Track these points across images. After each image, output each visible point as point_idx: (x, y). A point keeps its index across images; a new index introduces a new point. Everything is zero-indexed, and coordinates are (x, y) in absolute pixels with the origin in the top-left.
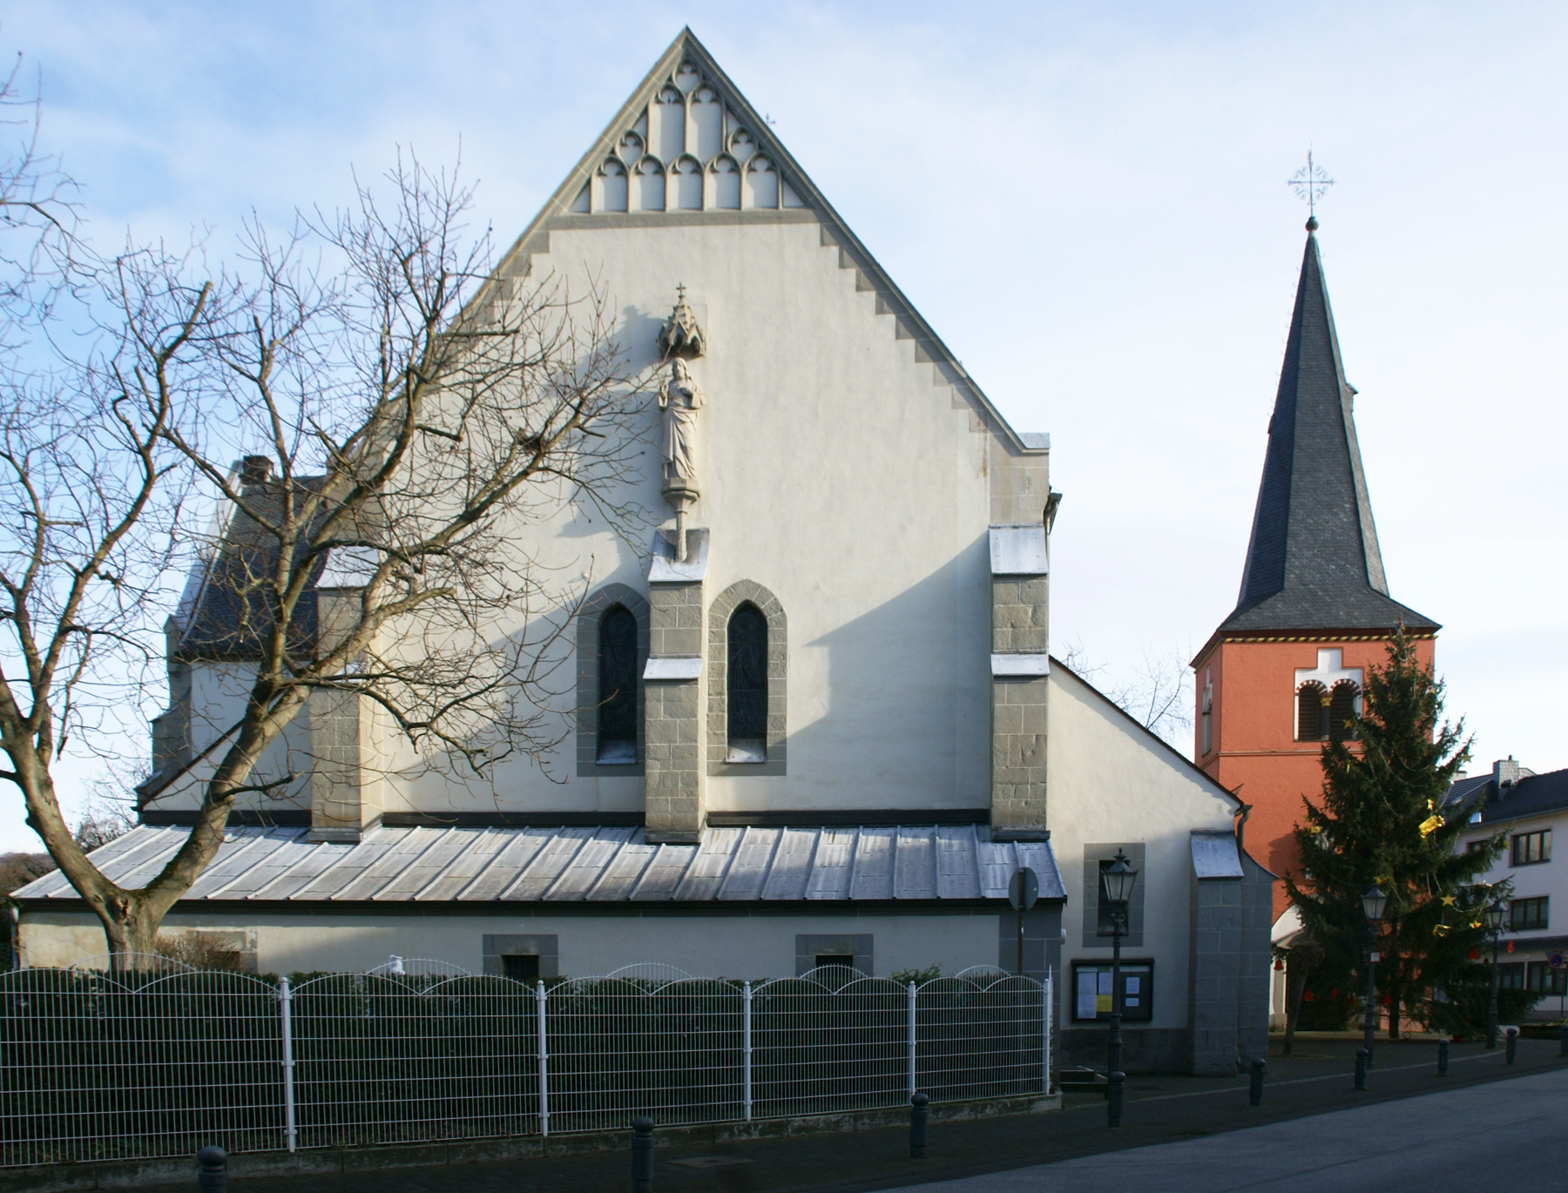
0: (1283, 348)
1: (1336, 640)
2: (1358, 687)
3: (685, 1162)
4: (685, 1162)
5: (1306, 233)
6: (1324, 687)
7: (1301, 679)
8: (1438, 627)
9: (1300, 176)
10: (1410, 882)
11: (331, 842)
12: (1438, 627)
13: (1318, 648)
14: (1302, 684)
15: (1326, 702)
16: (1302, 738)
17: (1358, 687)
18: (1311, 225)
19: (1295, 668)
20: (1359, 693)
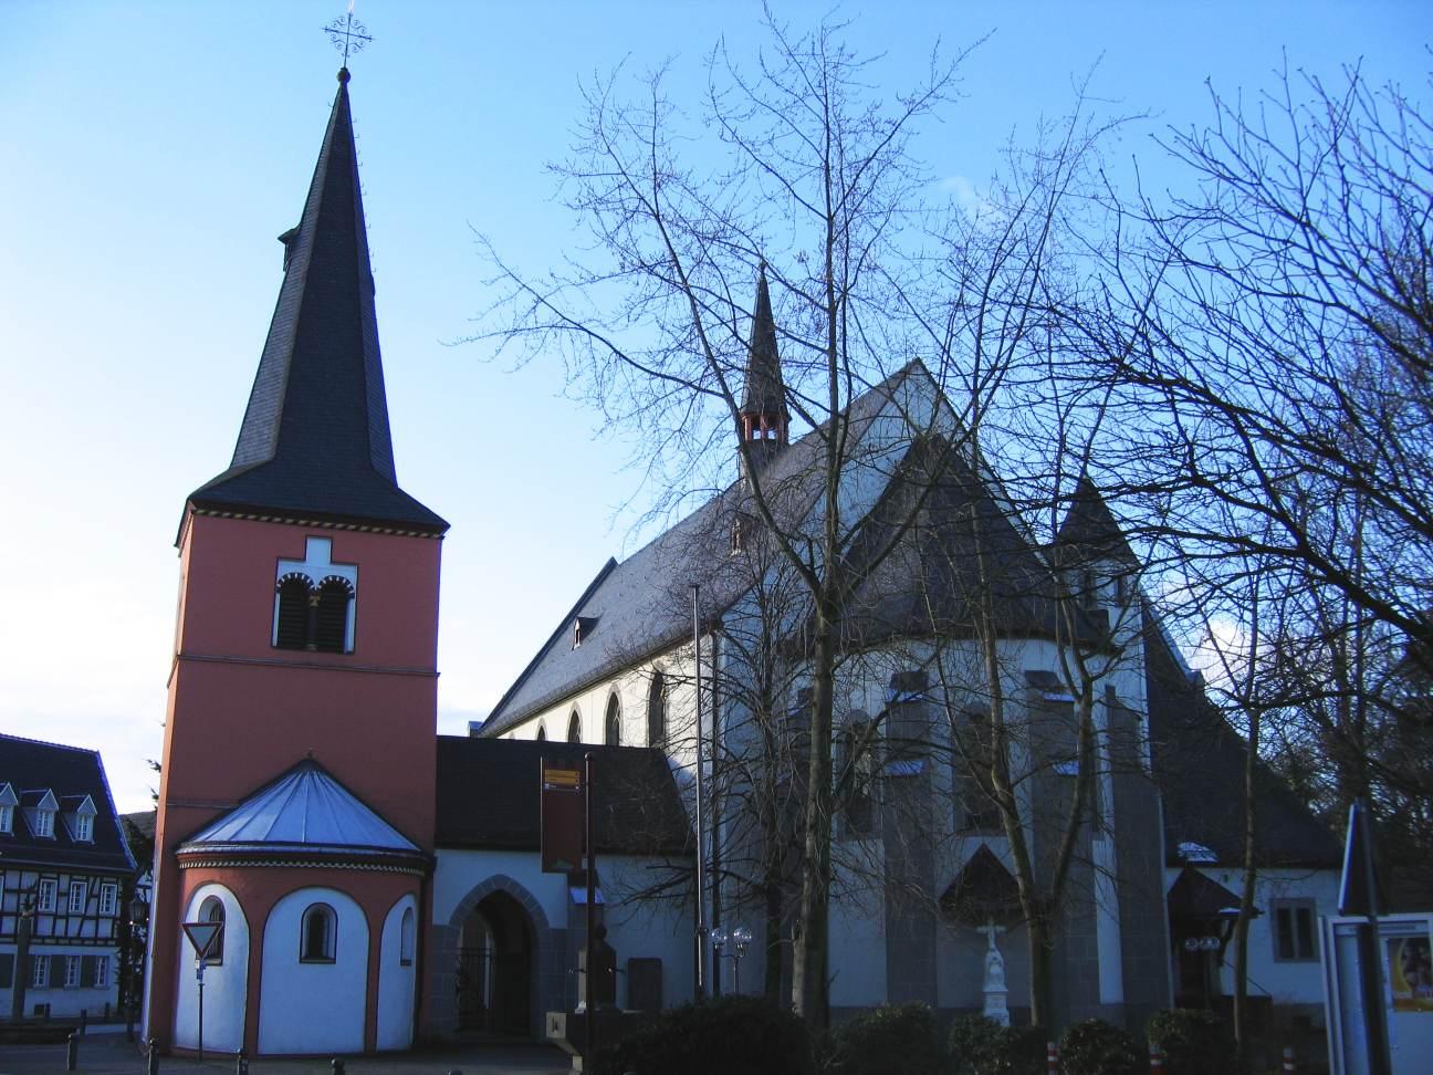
5: (338, 85)
7: (286, 569)
12: (446, 526)
16: (282, 644)
17: (352, 588)
18: (344, 76)
19: (279, 558)
20: (352, 596)
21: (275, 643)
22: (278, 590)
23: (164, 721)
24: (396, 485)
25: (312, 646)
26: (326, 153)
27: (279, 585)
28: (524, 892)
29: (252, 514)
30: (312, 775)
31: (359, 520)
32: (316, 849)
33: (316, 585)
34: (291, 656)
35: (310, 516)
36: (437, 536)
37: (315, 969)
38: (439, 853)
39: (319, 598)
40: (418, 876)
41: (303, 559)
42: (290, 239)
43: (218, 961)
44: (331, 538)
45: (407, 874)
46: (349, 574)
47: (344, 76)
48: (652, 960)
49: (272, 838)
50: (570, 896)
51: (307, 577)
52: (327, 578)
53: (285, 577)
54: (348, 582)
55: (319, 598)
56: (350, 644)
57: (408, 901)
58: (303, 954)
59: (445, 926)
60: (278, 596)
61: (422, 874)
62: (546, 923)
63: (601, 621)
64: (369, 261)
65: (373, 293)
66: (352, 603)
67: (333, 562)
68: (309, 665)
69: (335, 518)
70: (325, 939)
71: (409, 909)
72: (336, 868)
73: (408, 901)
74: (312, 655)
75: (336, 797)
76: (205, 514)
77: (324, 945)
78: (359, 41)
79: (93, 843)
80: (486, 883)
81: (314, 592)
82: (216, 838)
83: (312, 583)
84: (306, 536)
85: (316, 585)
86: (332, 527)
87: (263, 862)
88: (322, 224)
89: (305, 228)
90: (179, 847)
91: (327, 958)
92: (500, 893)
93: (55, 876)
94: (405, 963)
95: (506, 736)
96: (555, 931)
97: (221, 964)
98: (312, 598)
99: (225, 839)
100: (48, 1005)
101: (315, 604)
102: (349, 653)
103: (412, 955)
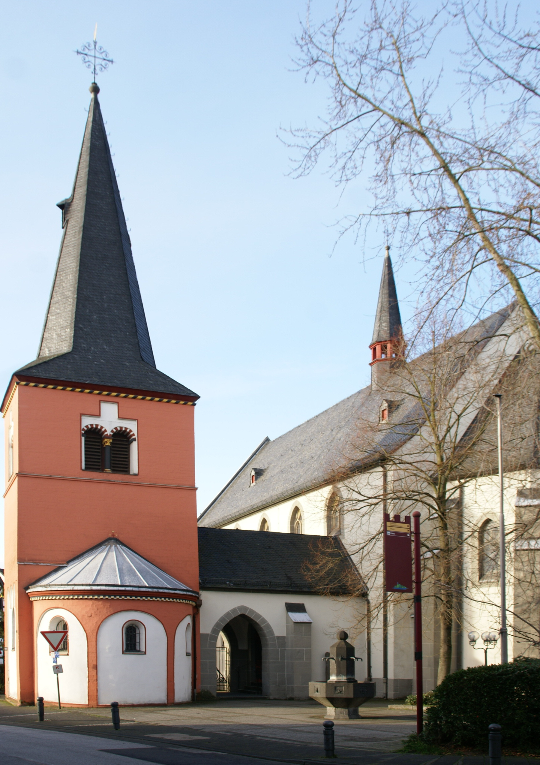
0: (123, 195)
1: (108, 395)
2: (134, 435)
3: (151, 736)
4: (151, 736)
5: (92, 96)
6: (105, 431)
7: (87, 422)
8: (197, 397)
9: (104, 65)
10: (395, 587)
11: (450, 573)
12: (197, 397)
13: (100, 401)
14: (112, 431)
15: (108, 442)
16: (87, 468)
17: (134, 435)
18: (96, 90)
19: (81, 415)
20: (135, 440)
21: (83, 467)
22: (83, 435)
23: (66, 195)
24: (155, 368)
25: (109, 470)
26: (88, 144)
27: (83, 432)
28: (259, 616)
29: (61, 386)
30: (116, 546)
31: (137, 392)
32: (155, 590)
33: (109, 433)
35: (101, 388)
36: (191, 403)
37: (131, 658)
38: (201, 592)
39: (111, 441)
40: (192, 605)
41: (99, 416)
42: (4, 607)
43: (66, 653)
44: (118, 403)
45: (188, 604)
46: (132, 426)
47: (96, 90)
49: (98, 582)
50: (288, 617)
53: (87, 426)
55: (111, 441)
56: (134, 467)
57: (188, 620)
58: (124, 649)
60: (83, 438)
61: (194, 604)
62: (272, 632)
63: (265, 473)
64: (125, 223)
65: (130, 245)
66: (134, 447)
67: (119, 418)
68: (108, 482)
69: (119, 390)
71: (189, 624)
72: (154, 600)
74: (108, 475)
75: (129, 558)
78: (104, 63)
81: (107, 437)
82: (57, 582)
83: (105, 431)
86: (117, 396)
87: (136, 597)
88: (91, 183)
89: (77, 196)
90: (28, 588)
91: (140, 651)
94: (188, 654)
95: (231, 527)
96: (279, 638)
97: (68, 655)
98: (106, 440)
99: (66, 583)
101: (108, 444)
103: (190, 650)
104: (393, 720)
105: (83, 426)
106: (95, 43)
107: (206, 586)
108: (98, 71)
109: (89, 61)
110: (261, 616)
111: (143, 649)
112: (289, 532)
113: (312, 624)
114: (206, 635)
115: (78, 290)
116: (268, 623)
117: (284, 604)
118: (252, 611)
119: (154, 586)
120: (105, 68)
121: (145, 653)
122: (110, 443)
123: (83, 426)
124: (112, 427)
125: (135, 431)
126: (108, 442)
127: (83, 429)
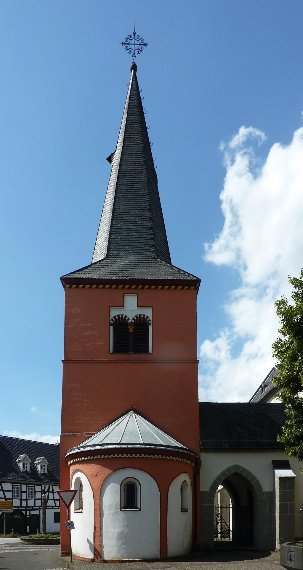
7: (115, 313)
12: (198, 281)
14: (133, 319)
15: (131, 329)
16: (117, 350)
17: (150, 320)
18: (134, 68)
19: (110, 306)
20: (150, 324)
21: (111, 350)
22: (112, 324)
28: (249, 473)
34: (119, 356)
39: (133, 327)
41: (124, 306)
44: (137, 294)
46: (148, 313)
47: (134, 68)
48: (55, 522)
51: (126, 317)
52: (136, 316)
53: (115, 317)
54: (147, 317)
56: (150, 350)
59: (207, 492)
60: (111, 327)
62: (261, 488)
66: (150, 327)
70: (136, 498)
73: (184, 477)
76: (70, 287)
77: (136, 501)
79: (30, 472)
80: (229, 469)
83: (129, 319)
84: (124, 294)
85: (131, 320)
91: (137, 508)
92: (236, 474)
93: (19, 485)
96: (267, 493)
97: (82, 512)
100: (188, 511)
102: (150, 354)
104: (110, 338)
105: (112, 317)
106: (135, 34)
107: (207, 448)
108: (136, 54)
109: (130, 48)
110: (252, 474)
111: (139, 506)
112: (301, 569)
113: (295, 480)
114: (206, 492)
115: (113, 210)
116: (258, 480)
117: (271, 461)
118: (244, 470)
119: (147, 443)
120: (141, 51)
121: (140, 510)
122: (132, 329)
123: (112, 317)
124: (134, 315)
125: (150, 317)
126: (131, 329)
127: (112, 320)
